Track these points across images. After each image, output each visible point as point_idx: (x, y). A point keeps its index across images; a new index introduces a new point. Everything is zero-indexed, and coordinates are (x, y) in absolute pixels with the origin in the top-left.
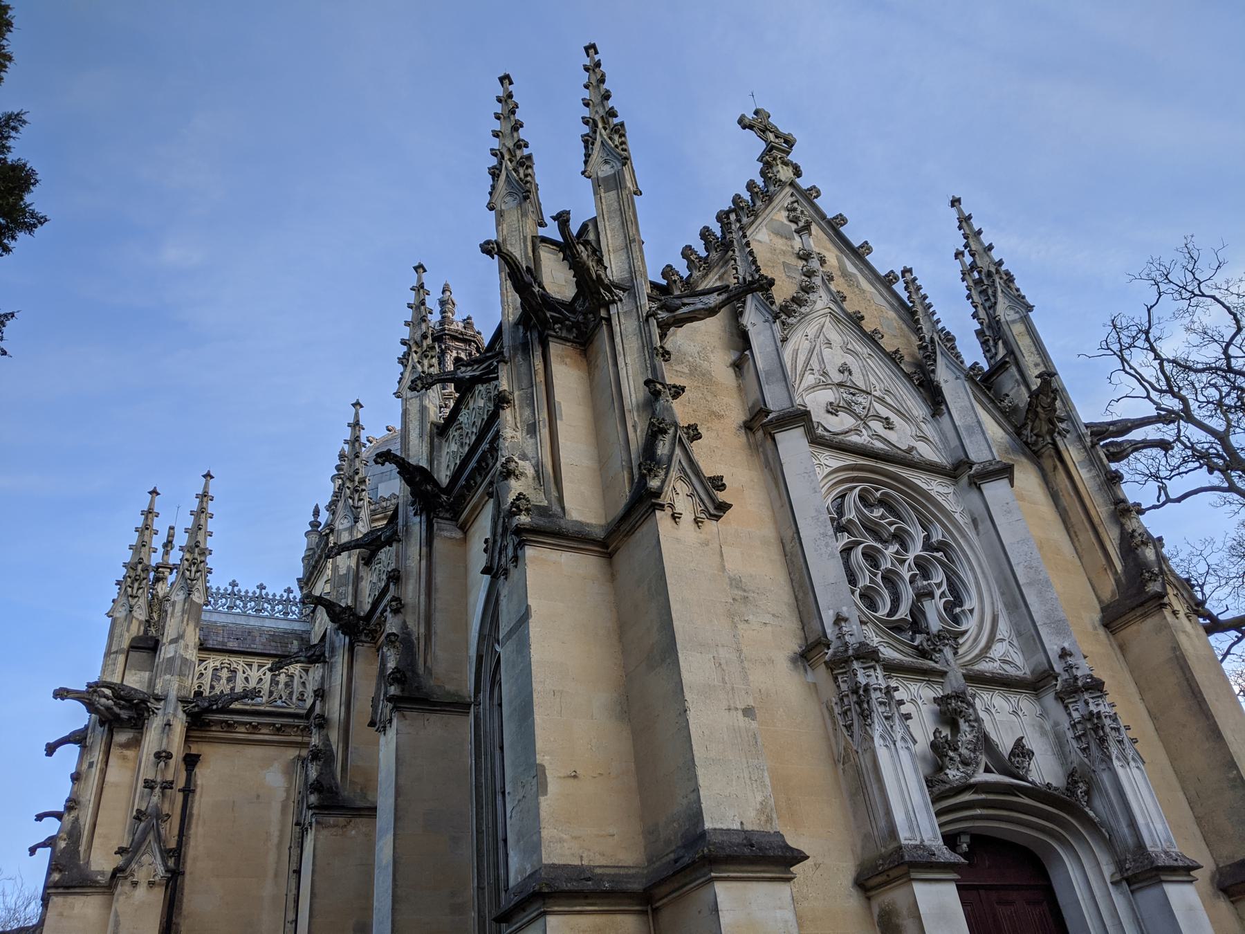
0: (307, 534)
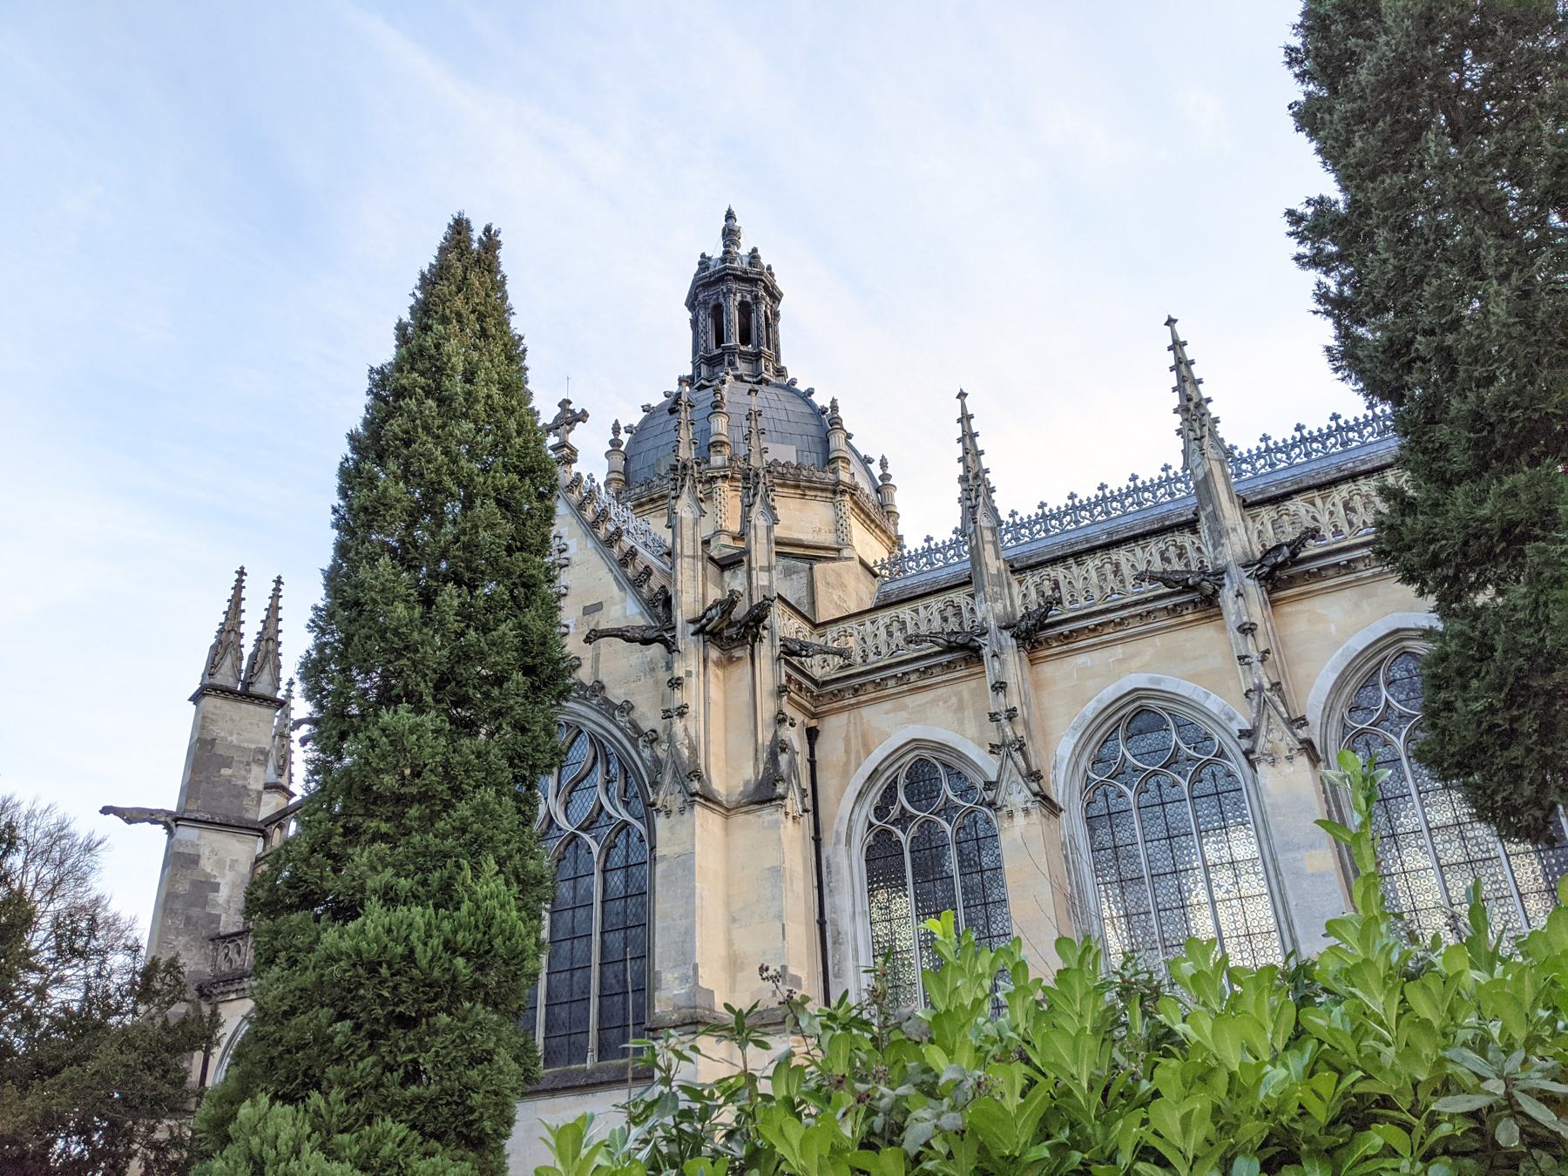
0: (608, 454)
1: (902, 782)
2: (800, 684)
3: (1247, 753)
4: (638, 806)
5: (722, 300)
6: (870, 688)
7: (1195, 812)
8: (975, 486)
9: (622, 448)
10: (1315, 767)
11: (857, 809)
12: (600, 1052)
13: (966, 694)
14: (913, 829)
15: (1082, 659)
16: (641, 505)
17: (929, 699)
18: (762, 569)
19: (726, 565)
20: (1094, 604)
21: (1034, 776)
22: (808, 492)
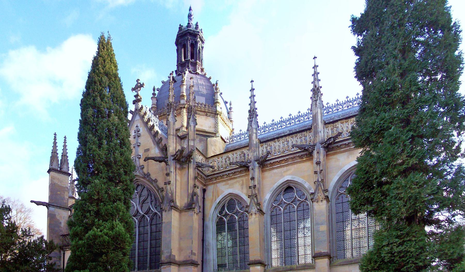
1: (226, 205)
2: (201, 176)
3: (311, 199)
4: (159, 208)
5: (185, 42)
6: (214, 179)
7: (297, 215)
8: (253, 114)
9: (156, 96)
10: (328, 203)
11: (215, 212)
12: (138, 269)
13: (244, 181)
14: (228, 217)
15: (275, 171)
16: (161, 116)
17: (234, 182)
18: (192, 140)
19: (182, 138)
20: (280, 154)
21: (258, 204)
22: (208, 114)
